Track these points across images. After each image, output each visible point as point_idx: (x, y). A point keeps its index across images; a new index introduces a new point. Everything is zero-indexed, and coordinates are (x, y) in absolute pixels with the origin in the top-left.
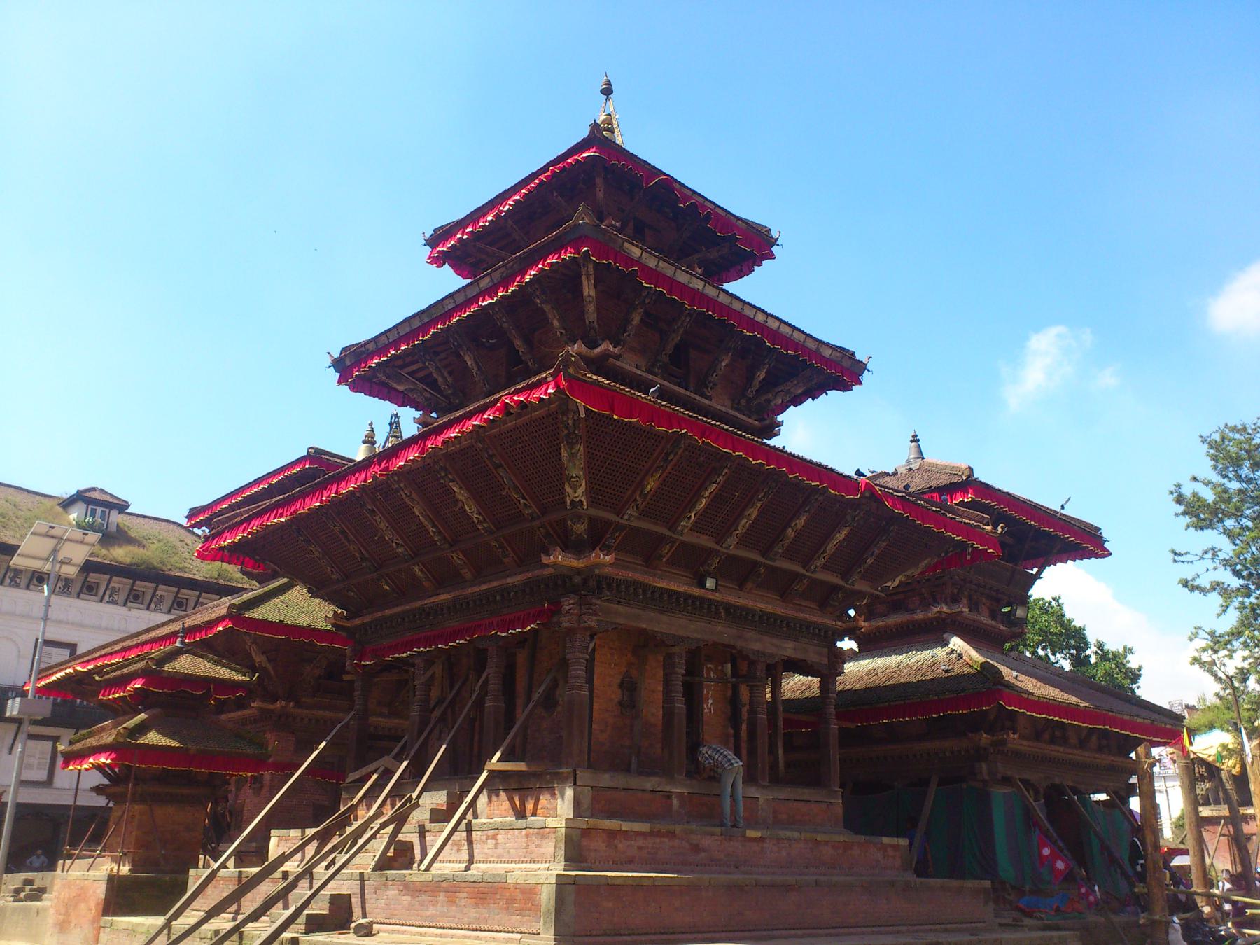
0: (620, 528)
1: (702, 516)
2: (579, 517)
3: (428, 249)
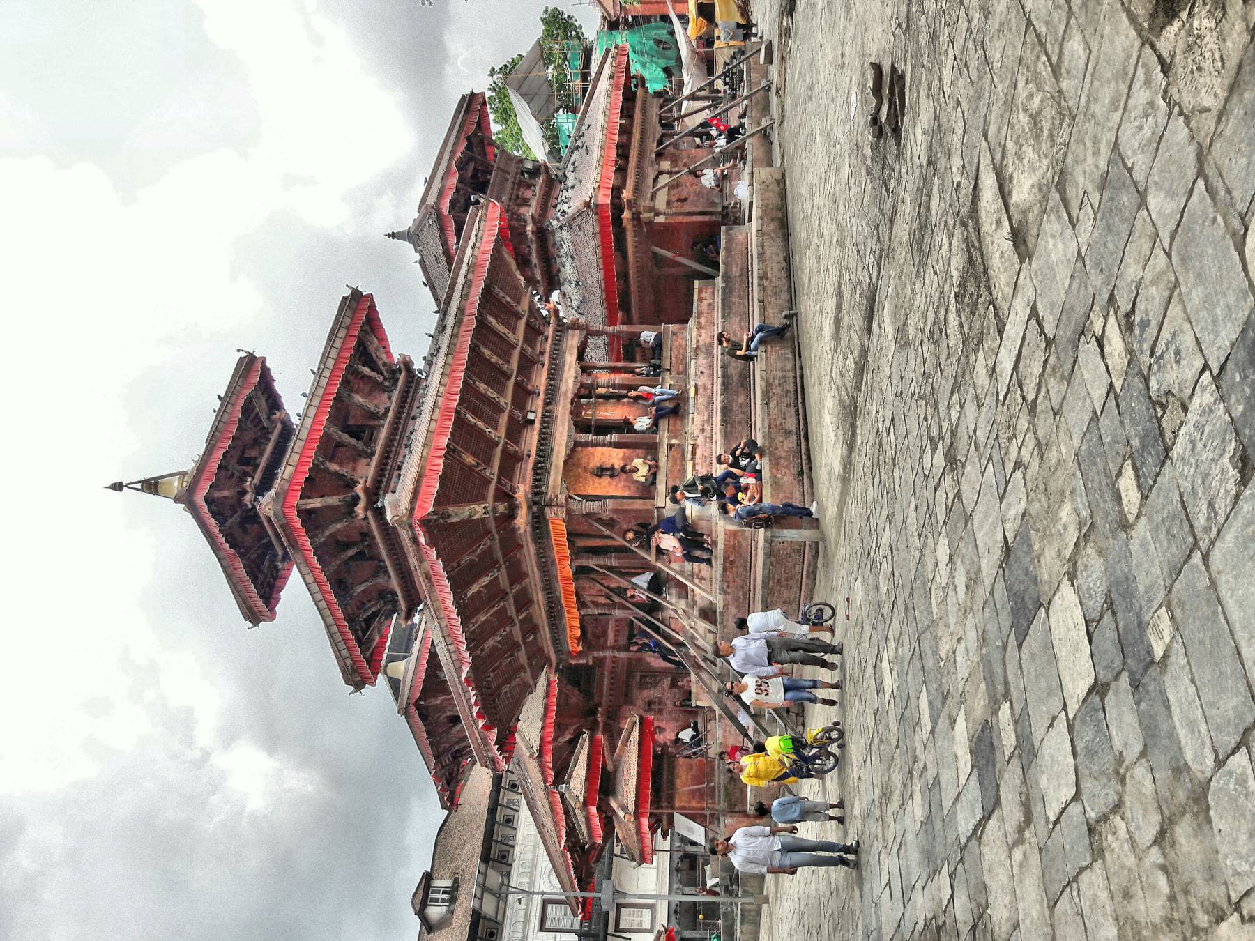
0: (499, 481)
2: (494, 509)
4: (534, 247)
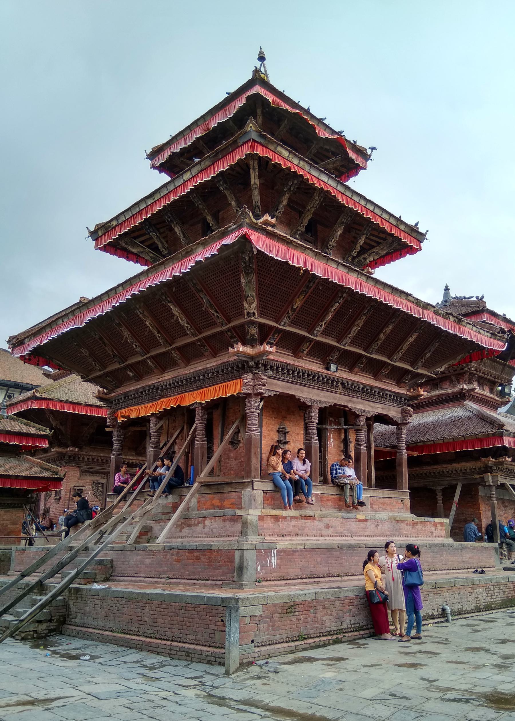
1: (330, 324)
3: (149, 162)
4: (449, 391)
